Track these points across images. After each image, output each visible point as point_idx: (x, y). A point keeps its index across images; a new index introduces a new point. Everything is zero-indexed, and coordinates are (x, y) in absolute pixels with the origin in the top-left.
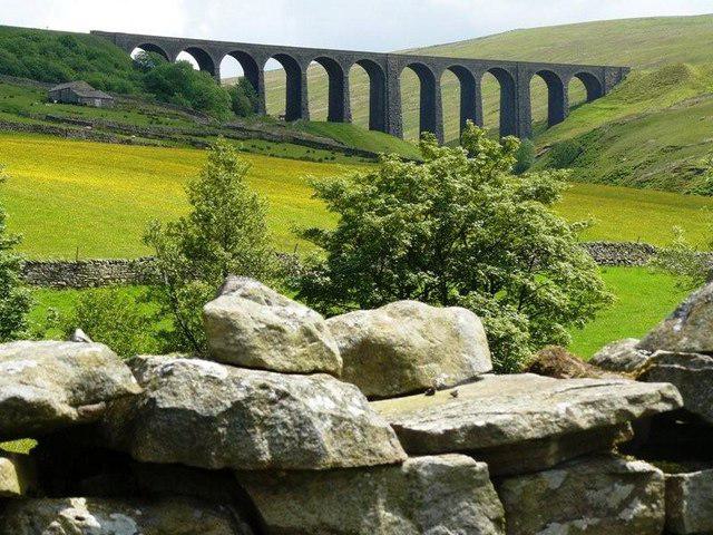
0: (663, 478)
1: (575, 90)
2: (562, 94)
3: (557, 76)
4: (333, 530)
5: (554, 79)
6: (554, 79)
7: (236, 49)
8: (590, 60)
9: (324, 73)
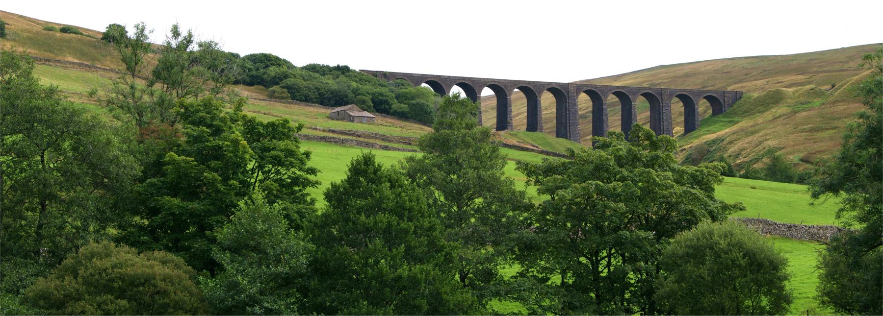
0: (536, 203)
1: (703, 107)
2: (694, 111)
3: (535, 94)
4: (496, 314)
5: (687, 100)
6: (687, 100)
7: (460, 81)
8: (713, 87)
9: (522, 95)
